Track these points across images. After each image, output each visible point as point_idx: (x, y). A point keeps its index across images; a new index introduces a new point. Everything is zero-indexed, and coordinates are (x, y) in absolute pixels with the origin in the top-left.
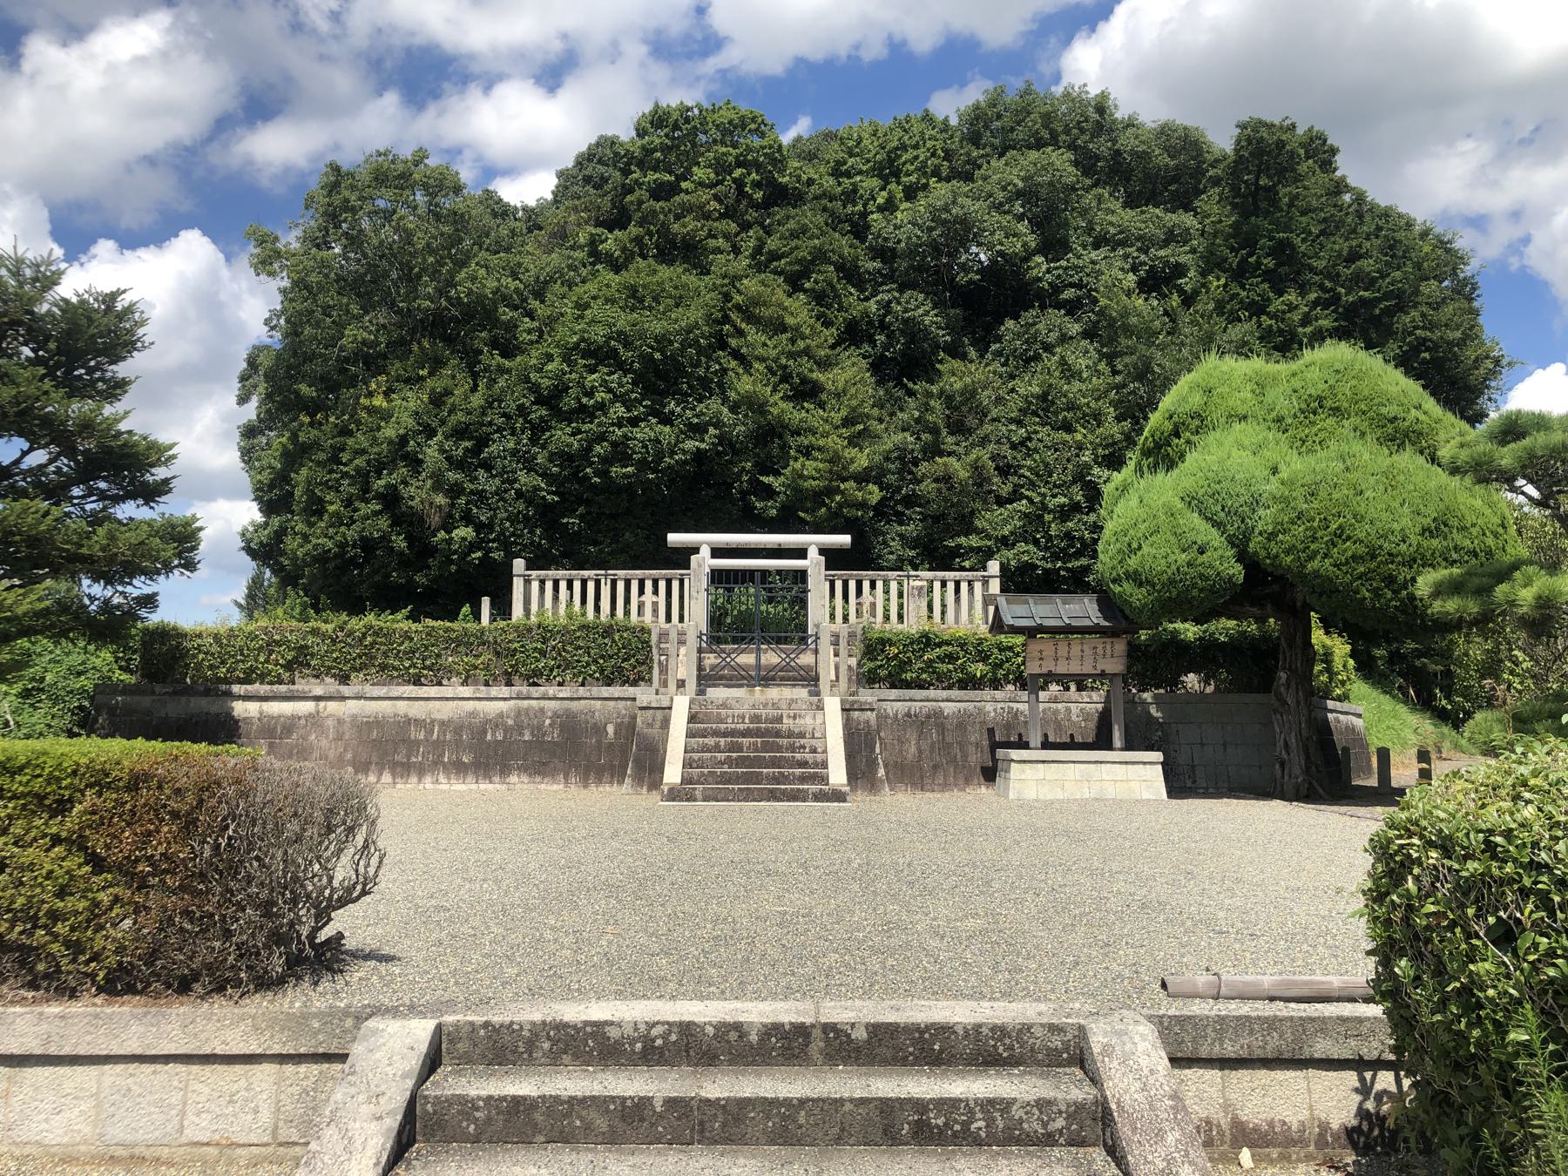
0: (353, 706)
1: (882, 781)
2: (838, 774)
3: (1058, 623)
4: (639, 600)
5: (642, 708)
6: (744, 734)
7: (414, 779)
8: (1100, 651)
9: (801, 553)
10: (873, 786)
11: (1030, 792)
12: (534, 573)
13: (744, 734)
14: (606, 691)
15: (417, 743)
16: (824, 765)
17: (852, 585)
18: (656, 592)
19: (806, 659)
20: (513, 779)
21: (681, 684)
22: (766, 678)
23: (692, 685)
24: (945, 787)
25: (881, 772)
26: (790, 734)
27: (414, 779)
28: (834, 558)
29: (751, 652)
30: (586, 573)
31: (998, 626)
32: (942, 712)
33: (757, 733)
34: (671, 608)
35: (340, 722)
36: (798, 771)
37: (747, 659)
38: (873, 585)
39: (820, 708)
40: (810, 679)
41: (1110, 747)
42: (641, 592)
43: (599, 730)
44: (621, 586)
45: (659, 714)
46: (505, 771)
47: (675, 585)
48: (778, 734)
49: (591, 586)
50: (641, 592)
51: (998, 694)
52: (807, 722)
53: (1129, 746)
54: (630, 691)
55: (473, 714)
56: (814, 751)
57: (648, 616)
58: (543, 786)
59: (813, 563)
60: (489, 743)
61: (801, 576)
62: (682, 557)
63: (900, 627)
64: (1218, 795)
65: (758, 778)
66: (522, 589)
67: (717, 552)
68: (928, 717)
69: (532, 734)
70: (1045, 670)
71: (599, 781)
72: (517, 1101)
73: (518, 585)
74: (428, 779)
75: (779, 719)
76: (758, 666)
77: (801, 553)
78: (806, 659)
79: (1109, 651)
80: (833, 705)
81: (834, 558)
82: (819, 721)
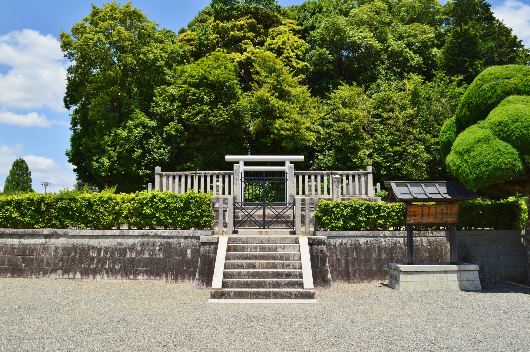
0: (62, 241)
2: (308, 282)
3: (424, 197)
5: (204, 244)
7: (91, 277)
9: (283, 164)
11: (411, 288)
12: (164, 173)
14: (186, 233)
15: (93, 258)
16: (301, 276)
20: (140, 277)
24: (361, 281)
26: (281, 258)
27: (91, 277)
28: (297, 166)
32: (358, 242)
34: (225, 190)
35: (57, 248)
39: (297, 241)
40: (290, 223)
43: (183, 252)
45: (212, 247)
46: (136, 274)
51: (387, 233)
52: (290, 251)
54: (199, 233)
55: (121, 244)
58: (155, 281)
59: (288, 168)
61: (283, 173)
62: (230, 166)
66: (159, 180)
67: (246, 164)
69: (150, 254)
71: (183, 278)
74: (98, 277)
76: (264, 216)
77: (283, 164)
79: (449, 211)
80: (304, 241)
81: (297, 166)
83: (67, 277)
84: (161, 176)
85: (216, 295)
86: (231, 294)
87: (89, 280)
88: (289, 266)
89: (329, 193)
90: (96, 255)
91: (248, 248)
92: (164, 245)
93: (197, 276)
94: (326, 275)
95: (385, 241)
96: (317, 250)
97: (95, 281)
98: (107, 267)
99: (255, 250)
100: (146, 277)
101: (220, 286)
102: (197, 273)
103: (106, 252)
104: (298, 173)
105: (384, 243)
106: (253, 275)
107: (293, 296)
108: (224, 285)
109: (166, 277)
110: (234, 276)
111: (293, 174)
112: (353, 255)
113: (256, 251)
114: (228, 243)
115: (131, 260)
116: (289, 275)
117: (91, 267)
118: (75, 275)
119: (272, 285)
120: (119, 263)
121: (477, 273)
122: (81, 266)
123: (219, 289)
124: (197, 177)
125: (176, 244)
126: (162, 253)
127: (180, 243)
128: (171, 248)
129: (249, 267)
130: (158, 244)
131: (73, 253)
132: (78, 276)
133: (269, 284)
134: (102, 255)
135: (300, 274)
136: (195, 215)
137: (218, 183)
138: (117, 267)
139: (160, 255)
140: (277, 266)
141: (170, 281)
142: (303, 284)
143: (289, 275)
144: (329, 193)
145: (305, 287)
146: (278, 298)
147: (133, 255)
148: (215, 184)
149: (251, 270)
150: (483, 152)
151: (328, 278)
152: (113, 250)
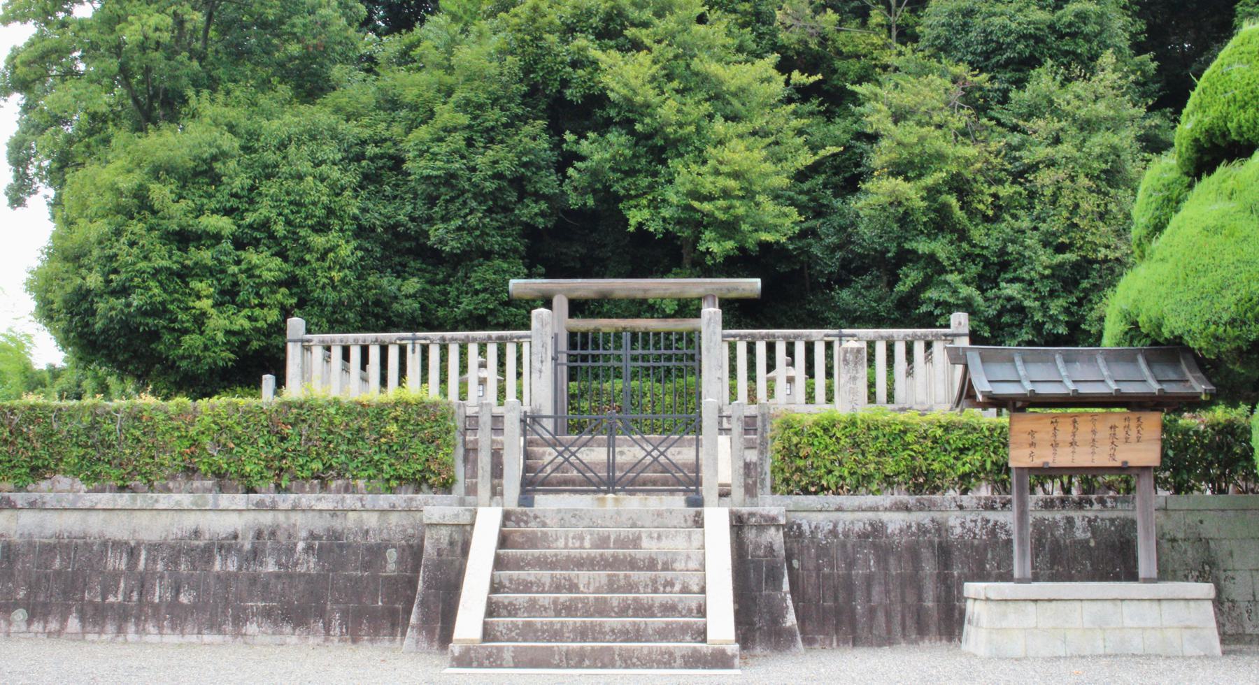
1: (790, 633)
2: (721, 625)
6: (580, 564)
7: (110, 628)
8: (1120, 433)
9: (688, 308)
10: (778, 639)
12: (316, 337)
13: (580, 564)
15: (116, 575)
17: (761, 348)
20: (252, 628)
22: (610, 482)
25: (791, 619)
26: (651, 565)
27: (110, 628)
31: (967, 394)
32: (883, 526)
33: (605, 564)
36: (659, 621)
37: (595, 455)
39: (699, 522)
40: (688, 484)
41: (1132, 576)
42: (771, 366)
44: (434, 354)
46: (240, 619)
47: (511, 350)
48: (633, 565)
49: (393, 353)
50: (771, 366)
52: (676, 543)
53: (1165, 573)
56: (685, 590)
60: (218, 576)
65: (638, 635)
66: (298, 360)
68: (864, 536)
70: (1037, 462)
71: (375, 633)
75: (635, 542)
76: (611, 466)
78: (682, 454)
80: (717, 519)
82: (696, 544)
83: (41, 629)
84: (307, 348)
85: (464, 660)
86: (508, 656)
87: (104, 637)
88: (672, 585)
89: (830, 399)
90: (123, 567)
91: (557, 540)
92: (320, 538)
93: (413, 619)
94: (782, 615)
95: (963, 525)
96: (757, 546)
97: (121, 639)
98: (157, 601)
99: (577, 545)
100: (268, 627)
101: (477, 634)
102: (415, 609)
103: (152, 559)
104: (734, 336)
105: (958, 530)
106: (569, 609)
107: (679, 661)
108: (488, 634)
109: (327, 629)
110: (515, 609)
111: (720, 338)
112: (869, 567)
113: (582, 547)
114: (504, 525)
115: (225, 580)
116: (669, 609)
117: (111, 599)
118: (64, 620)
119: (621, 631)
120: (191, 588)
121: (1209, 608)
122: (83, 598)
123: (472, 641)
124: (418, 349)
125: (356, 534)
126: (313, 560)
127: (367, 532)
128: (341, 546)
129: (558, 588)
130: (304, 534)
131: (58, 561)
132: (73, 624)
133: (613, 631)
134: (141, 565)
135: (700, 606)
136: (414, 451)
137: (483, 373)
138: (184, 599)
139: (310, 565)
140: (637, 585)
141: (336, 640)
142: (705, 630)
143: (669, 609)
144: (830, 399)
145: (710, 636)
146: (634, 666)
147: (232, 566)
148: (473, 373)
149: (563, 596)
150: (745, 227)
151: (788, 624)
152: (175, 551)
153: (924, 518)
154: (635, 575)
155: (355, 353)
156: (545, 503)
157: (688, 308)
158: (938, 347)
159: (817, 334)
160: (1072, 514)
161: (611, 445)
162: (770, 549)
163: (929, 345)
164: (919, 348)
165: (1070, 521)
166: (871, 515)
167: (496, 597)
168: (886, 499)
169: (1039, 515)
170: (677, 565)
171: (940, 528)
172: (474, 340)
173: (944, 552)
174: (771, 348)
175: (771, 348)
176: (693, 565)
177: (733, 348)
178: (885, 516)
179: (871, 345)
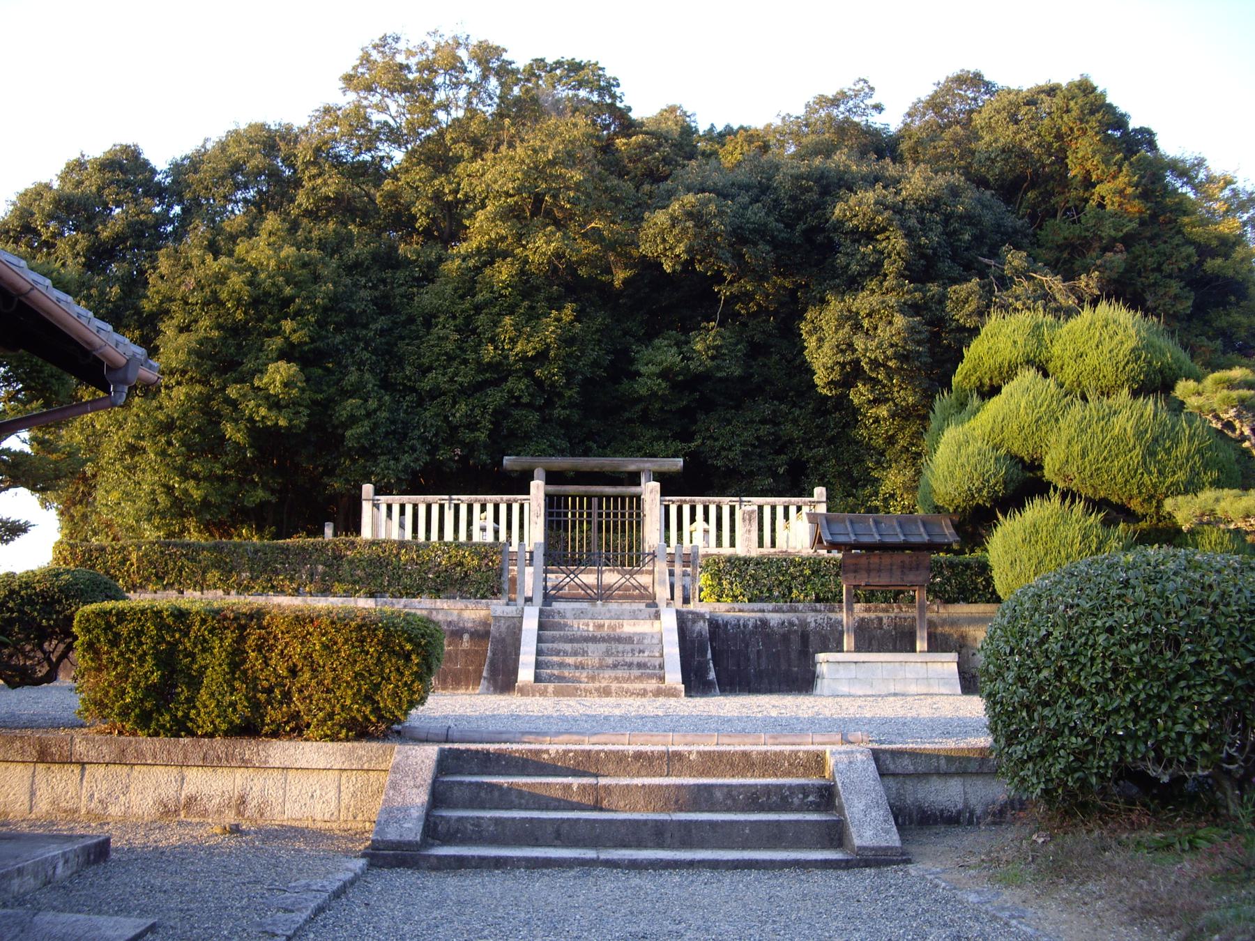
2: (674, 677)
4: (476, 520)
18: (706, 520)
19: (644, 579)
21: (529, 600)
23: (539, 599)
25: (712, 675)
29: (591, 572)
30: (430, 498)
37: (589, 579)
38: (483, 509)
41: (842, 651)
42: (693, 520)
48: (619, 640)
50: (693, 520)
57: (698, 539)
63: (773, 550)
64: (770, 691)
72: (637, 821)
73: (367, 507)
78: (644, 579)
94: (707, 671)
108: (538, 679)
144: (733, 545)
153: (793, 617)
154: (621, 647)
155: (396, 510)
156: (557, 606)
157: (634, 479)
158: (805, 509)
159: (726, 502)
160: (881, 615)
161: (600, 572)
162: (700, 633)
163: (799, 509)
164: (793, 509)
165: (880, 619)
166: (759, 615)
167: (540, 658)
168: (770, 606)
169: (861, 615)
170: (646, 641)
171: (804, 624)
172: (685, 502)
173: (805, 637)
174: (693, 509)
175: (693, 509)
176: (655, 641)
177: (667, 508)
178: (769, 616)
179: (761, 508)
